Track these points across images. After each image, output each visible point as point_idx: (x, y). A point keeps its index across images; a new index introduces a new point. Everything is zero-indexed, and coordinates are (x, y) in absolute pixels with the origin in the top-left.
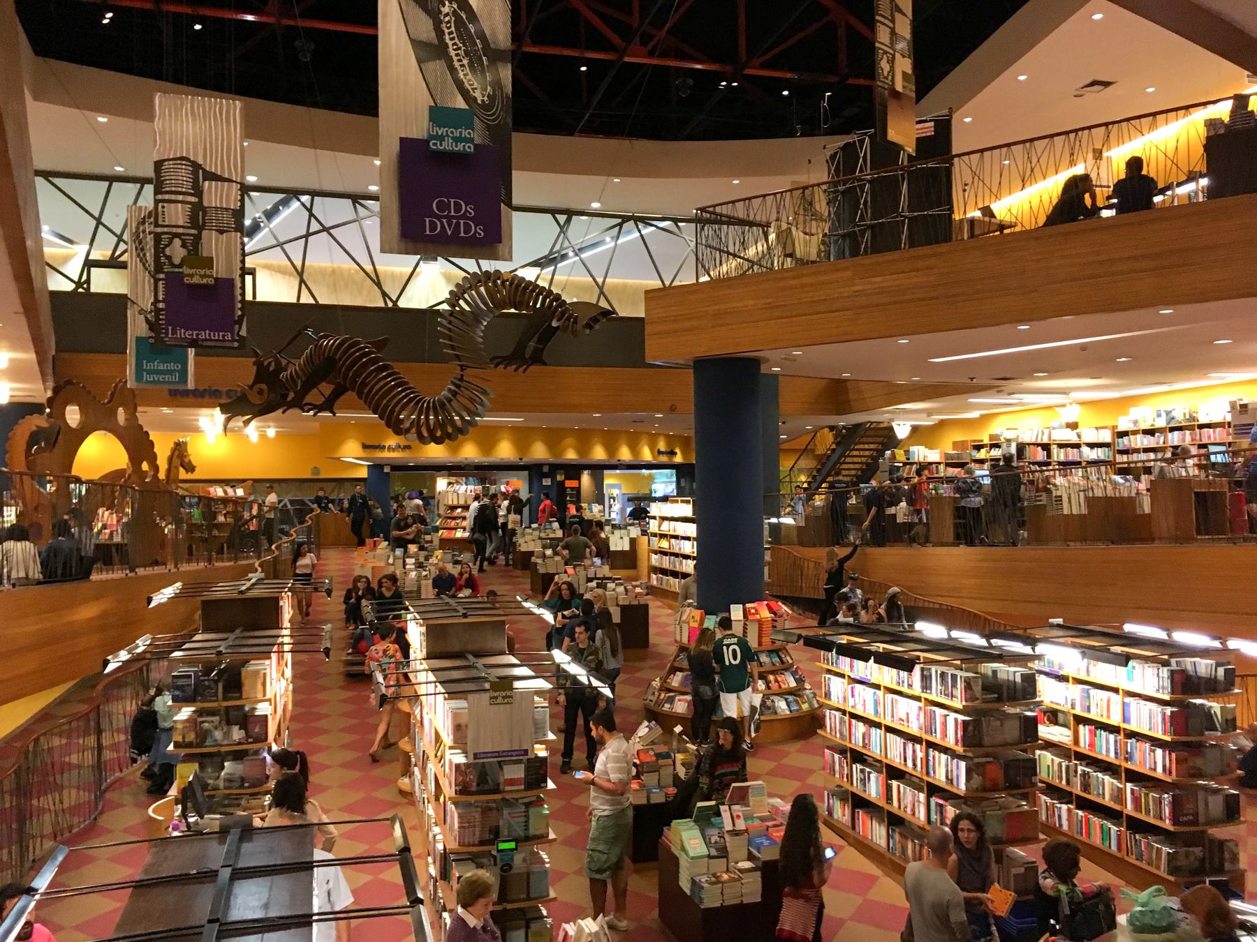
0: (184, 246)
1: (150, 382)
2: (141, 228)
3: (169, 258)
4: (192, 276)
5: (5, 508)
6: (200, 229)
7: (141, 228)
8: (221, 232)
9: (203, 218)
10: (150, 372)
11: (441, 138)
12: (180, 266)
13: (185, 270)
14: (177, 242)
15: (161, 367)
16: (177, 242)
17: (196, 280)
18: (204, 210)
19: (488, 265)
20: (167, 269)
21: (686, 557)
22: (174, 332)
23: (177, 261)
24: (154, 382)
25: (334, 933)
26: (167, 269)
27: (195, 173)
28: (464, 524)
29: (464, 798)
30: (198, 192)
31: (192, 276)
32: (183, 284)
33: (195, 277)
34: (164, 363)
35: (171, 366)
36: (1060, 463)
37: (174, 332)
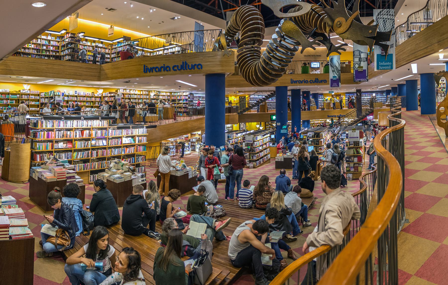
0: (358, 65)
1: (382, 69)
2: (378, 17)
6: (361, 62)
7: (378, 17)
9: (238, 192)
10: (382, 66)
13: (358, 69)
14: (357, 64)
16: (357, 64)
17: (360, 70)
18: (361, 58)
19: (129, 255)
23: (357, 67)
24: (383, 69)
27: (359, 52)
28: (56, 130)
30: (360, 55)
33: (360, 70)
35: (388, 63)
36: (149, 159)
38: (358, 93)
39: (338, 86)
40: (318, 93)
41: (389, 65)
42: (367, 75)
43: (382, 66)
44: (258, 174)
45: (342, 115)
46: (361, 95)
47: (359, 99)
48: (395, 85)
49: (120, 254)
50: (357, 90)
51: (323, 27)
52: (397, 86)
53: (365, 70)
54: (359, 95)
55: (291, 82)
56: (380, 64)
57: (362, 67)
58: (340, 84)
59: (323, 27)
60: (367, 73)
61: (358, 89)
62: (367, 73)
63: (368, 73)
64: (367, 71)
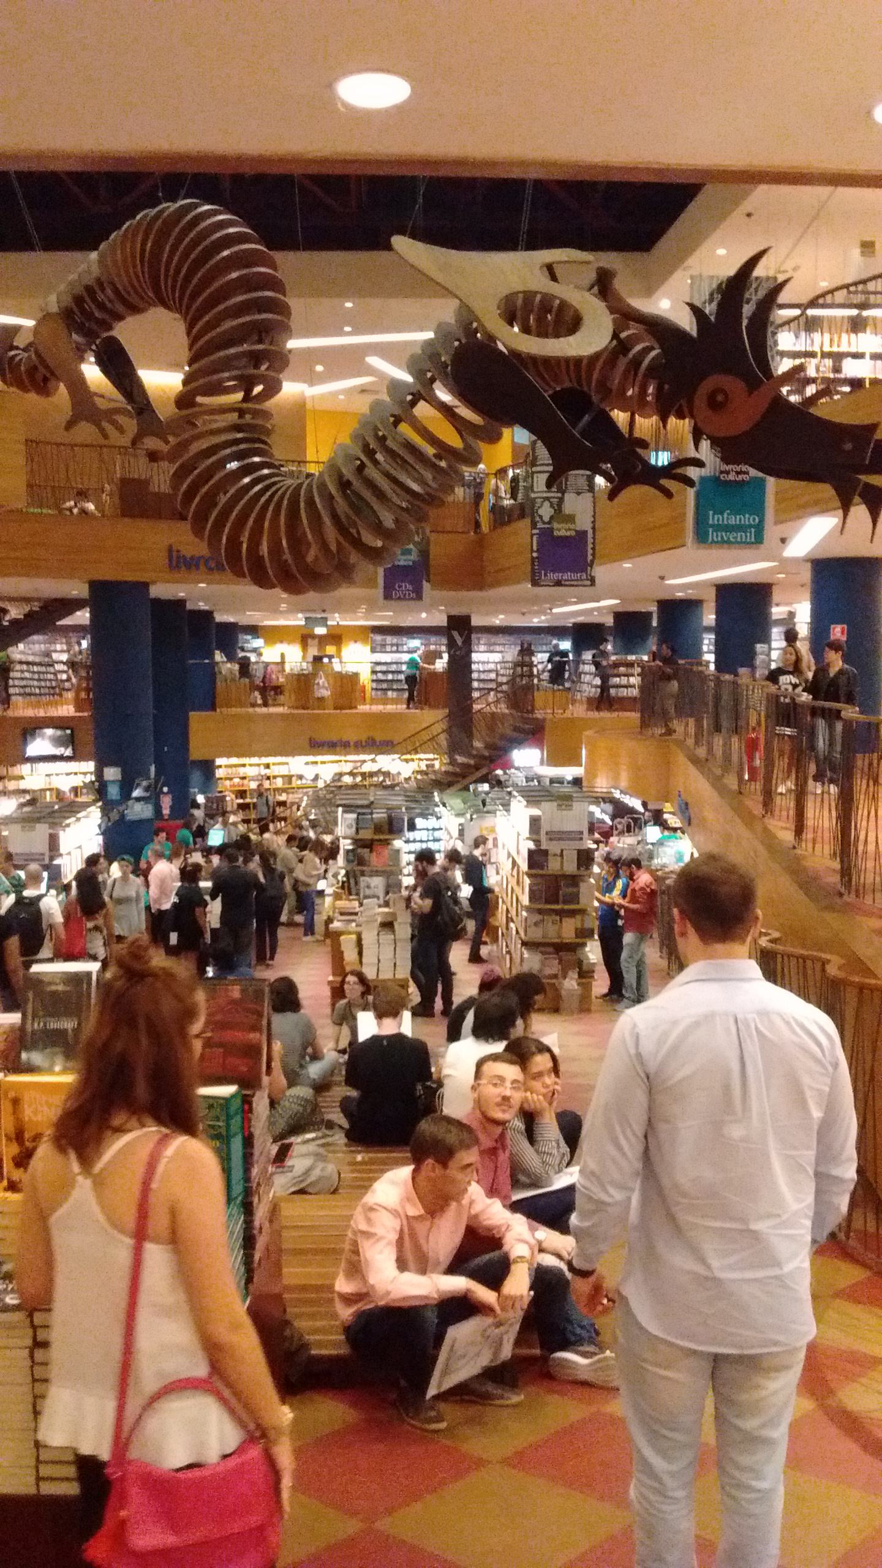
0: (552, 506)
3: (541, 517)
4: (559, 530)
5: (88, 622)
6: (563, 493)
8: (579, 494)
10: (718, 528)
11: (728, 473)
12: (549, 523)
15: (732, 521)
16: (547, 504)
17: (563, 533)
20: (540, 525)
21: (477, 689)
22: (546, 575)
23: (546, 519)
25: (441, 624)
26: (540, 525)
29: (533, 871)
31: (559, 530)
32: (553, 537)
33: (561, 530)
34: (735, 515)
37: (546, 575)
38: (455, 634)
39: (419, 597)
40: (234, 625)
41: (750, 526)
42: (590, 558)
43: (718, 528)
44: (35, 1057)
45: (378, 739)
46: (468, 642)
47: (461, 664)
48: (646, 600)
49: (33, 1375)
50: (450, 618)
51: (260, 294)
52: (653, 608)
53: (582, 534)
54: (459, 642)
55: (170, 565)
56: (713, 519)
57: (571, 519)
58: (426, 585)
59: (260, 294)
60: (590, 546)
61: (455, 612)
62: (590, 546)
63: (593, 549)
64: (590, 540)
